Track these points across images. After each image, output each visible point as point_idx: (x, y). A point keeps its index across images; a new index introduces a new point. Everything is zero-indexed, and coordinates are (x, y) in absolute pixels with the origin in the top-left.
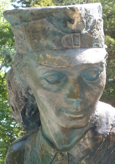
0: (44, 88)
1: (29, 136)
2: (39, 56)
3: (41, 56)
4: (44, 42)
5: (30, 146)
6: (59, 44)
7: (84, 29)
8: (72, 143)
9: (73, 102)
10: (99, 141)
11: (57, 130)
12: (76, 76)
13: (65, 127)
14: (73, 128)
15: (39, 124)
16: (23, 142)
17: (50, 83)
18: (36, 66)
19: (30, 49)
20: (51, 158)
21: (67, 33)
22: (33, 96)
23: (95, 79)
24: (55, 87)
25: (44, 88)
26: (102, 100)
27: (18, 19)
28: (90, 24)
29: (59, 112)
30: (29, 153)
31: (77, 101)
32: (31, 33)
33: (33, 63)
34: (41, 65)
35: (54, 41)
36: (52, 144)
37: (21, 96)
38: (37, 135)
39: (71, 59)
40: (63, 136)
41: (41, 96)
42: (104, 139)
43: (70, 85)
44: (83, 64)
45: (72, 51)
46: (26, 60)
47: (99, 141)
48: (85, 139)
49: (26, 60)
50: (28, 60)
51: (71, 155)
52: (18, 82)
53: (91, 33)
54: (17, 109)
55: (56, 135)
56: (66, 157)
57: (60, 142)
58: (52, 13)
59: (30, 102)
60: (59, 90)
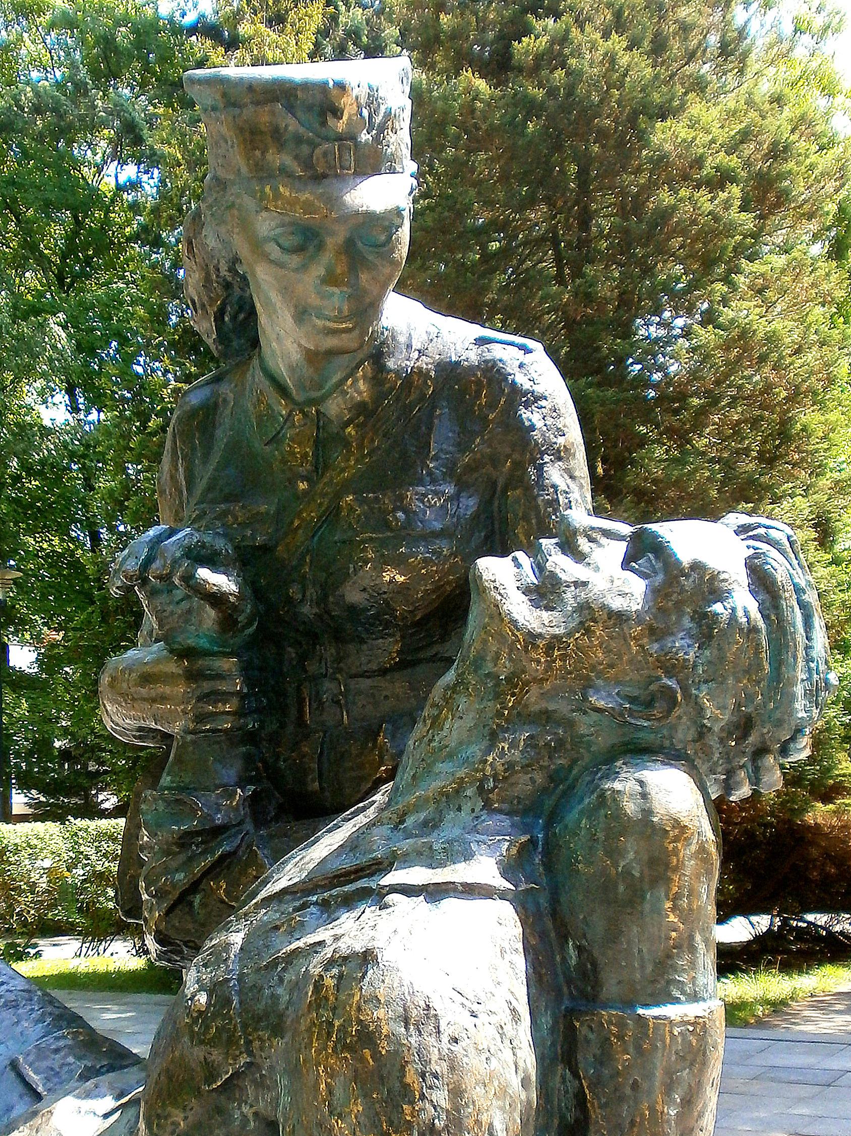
0: (271, 262)
1: (227, 372)
2: (264, 188)
3: (267, 189)
4: (276, 158)
5: (231, 395)
6: (308, 164)
7: (365, 131)
8: (327, 388)
9: (333, 294)
10: (387, 386)
11: (296, 356)
12: (340, 239)
13: (312, 348)
14: (331, 353)
15: (255, 343)
16: (211, 386)
17: (284, 249)
18: (257, 212)
19: (244, 170)
20: (278, 422)
21: (327, 139)
22: (244, 278)
23: (383, 245)
24: (295, 260)
25: (271, 262)
26: (401, 288)
27: (218, 97)
28: (378, 119)
29: (301, 314)
30: (228, 412)
31: (341, 292)
32: (247, 133)
33: (249, 203)
34: (266, 209)
35: (296, 157)
36: (282, 390)
37: (217, 276)
38: (248, 370)
39: (333, 202)
40: (308, 372)
41: (266, 277)
42: (399, 382)
43: (327, 257)
44: (357, 213)
45: (335, 181)
46: (232, 194)
47: (387, 386)
48: (355, 381)
49: (232, 194)
50: (238, 196)
51: (324, 415)
52: (212, 242)
53: (377, 140)
54: (203, 306)
55: (292, 369)
56: (313, 420)
57: (301, 386)
58: (295, 89)
59: (237, 291)
60: (303, 268)
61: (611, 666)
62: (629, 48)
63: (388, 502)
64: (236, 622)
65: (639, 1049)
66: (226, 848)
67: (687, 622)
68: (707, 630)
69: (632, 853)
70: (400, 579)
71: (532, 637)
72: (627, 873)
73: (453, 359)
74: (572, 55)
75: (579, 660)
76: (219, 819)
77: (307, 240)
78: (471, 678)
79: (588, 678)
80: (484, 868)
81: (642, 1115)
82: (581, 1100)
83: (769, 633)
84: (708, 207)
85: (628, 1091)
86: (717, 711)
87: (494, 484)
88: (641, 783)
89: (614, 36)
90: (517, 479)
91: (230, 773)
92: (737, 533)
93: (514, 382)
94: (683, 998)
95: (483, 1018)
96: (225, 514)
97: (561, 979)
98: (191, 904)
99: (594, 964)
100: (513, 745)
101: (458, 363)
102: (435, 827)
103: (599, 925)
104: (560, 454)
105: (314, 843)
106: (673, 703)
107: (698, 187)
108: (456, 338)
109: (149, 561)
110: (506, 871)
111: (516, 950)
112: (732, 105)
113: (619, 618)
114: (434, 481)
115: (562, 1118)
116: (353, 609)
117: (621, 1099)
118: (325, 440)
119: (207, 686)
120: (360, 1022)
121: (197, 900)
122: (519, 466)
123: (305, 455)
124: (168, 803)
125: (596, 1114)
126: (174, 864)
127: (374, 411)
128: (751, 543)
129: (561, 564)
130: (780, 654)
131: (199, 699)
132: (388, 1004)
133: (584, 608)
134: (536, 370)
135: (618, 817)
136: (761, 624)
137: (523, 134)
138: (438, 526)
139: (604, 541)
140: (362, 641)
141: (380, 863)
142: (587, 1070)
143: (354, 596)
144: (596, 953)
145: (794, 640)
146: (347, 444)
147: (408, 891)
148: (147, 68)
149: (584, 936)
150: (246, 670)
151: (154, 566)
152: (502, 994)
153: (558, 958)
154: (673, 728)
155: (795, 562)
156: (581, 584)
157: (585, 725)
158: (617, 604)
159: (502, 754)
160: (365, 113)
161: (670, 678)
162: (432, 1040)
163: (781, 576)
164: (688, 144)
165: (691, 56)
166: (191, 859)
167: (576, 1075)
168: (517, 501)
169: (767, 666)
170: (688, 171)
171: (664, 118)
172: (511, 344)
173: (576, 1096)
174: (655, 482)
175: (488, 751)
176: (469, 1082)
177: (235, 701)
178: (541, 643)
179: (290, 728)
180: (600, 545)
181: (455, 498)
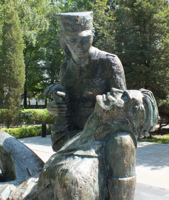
4: (69, 28)
6: (73, 29)
23: (88, 41)
24: (73, 44)
28: (85, 22)
35: (71, 28)
39: (77, 35)
40: (78, 60)
43: (77, 43)
48: (86, 61)
53: (85, 25)
55: (76, 59)
57: (77, 61)
62: (150, 4)
63: (90, 81)
65: (119, 185)
66: (63, 135)
67: (131, 109)
68: (135, 110)
69: (119, 151)
70: (91, 93)
71: (104, 110)
72: (118, 154)
74: (142, 5)
75: (112, 115)
76: (63, 130)
77: (74, 41)
79: (114, 118)
80: (93, 152)
81: (119, 197)
82: (109, 193)
83: (146, 111)
84: (162, 26)
86: (136, 124)
88: (121, 138)
89: (148, 2)
90: (111, 78)
91: (66, 123)
92: (142, 92)
93: (111, 62)
94: (127, 176)
95: (87, 183)
96: (66, 81)
97: (106, 171)
98: (58, 143)
100: (101, 129)
102: (87, 142)
104: (119, 74)
105: (72, 139)
106: (128, 123)
107: (160, 23)
109: (49, 91)
110: (96, 152)
112: (165, 12)
113: (119, 108)
114: (98, 78)
115: (106, 196)
116: (84, 97)
119: (61, 109)
120: (64, 183)
121: (59, 143)
122: (112, 75)
123: (78, 73)
125: (111, 196)
128: (144, 94)
129: (111, 97)
130: (148, 115)
131: (60, 111)
134: (117, 60)
136: (144, 110)
138: (98, 85)
139: (118, 93)
142: (110, 188)
143: (85, 96)
146: (85, 71)
147: (78, 156)
148: (86, 6)
149: (110, 164)
150: (68, 107)
151: (50, 91)
152: (92, 178)
153: (106, 168)
156: (113, 101)
157: (113, 126)
158: (119, 105)
161: (128, 119)
162: (76, 187)
163: (149, 101)
165: (160, 5)
166: (58, 136)
169: (145, 117)
170: (159, 21)
171: (155, 14)
172: (112, 56)
174: (154, 64)
175: (96, 129)
176: (83, 195)
177: (66, 111)
178: (106, 111)
180: (118, 94)
181: (101, 81)
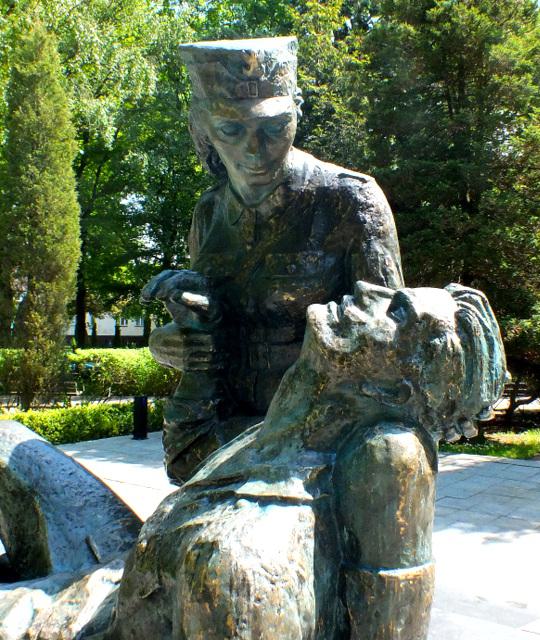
0: (221, 140)
6: (233, 92)
23: (280, 131)
24: (231, 139)
35: (228, 89)
36: (238, 197)
39: (246, 112)
43: (248, 138)
48: (275, 196)
55: (242, 189)
61: (376, 372)
62: (480, 13)
64: (208, 318)
65: (379, 592)
66: (202, 432)
67: (419, 349)
68: (430, 353)
69: (379, 482)
70: (292, 299)
71: (332, 353)
72: (376, 493)
73: (326, 185)
76: (200, 416)
77: (237, 130)
78: (303, 372)
79: (363, 378)
80: (296, 487)
83: (466, 356)
85: (373, 617)
86: (434, 398)
87: (344, 251)
88: (386, 442)
89: (473, 8)
90: (356, 248)
92: (453, 296)
93: (356, 199)
96: (212, 259)
97: (339, 548)
98: (185, 459)
99: (357, 542)
100: (321, 412)
101: (328, 188)
102: (277, 455)
103: (359, 523)
104: (381, 235)
105: (229, 446)
106: (409, 395)
107: (511, 75)
108: (330, 172)
109: (156, 290)
110: (308, 488)
111: (309, 537)
112: (529, 38)
113: (381, 345)
115: (338, 627)
116: (269, 312)
117: (369, 621)
118: (260, 225)
119: (195, 349)
120: (205, 586)
121: (188, 457)
122: (358, 242)
124: (176, 406)
126: (177, 438)
127: (284, 212)
128: (460, 302)
129: (353, 310)
132: (221, 576)
133: (362, 338)
134: (373, 194)
135: (372, 461)
136: (461, 351)
137: (430, 51)
138: (312, 272)
139: (378, 298)
140: (277, 328)
141: (242, 476)
143: (271, 306)
144: (358, 535)
145: (481, 359)
146: (270, 229)
147: (251, 498)
148: (274, 20)
150: (217, 342)
152: (293, 569)
153: (339, 537)
154: (411, 407)
155: (486, 313)
156: (362, 324)
157: (360, 402)
158: (379, 337)
159: (315, 417)
160: (264, 66)
161: (408, 380)
162: (244, 600)
163: (475, 323)
164: (507, 55)
165: (510, 17)
167: (345, 605)
168: (356, 259)
169: (464, 376)
170: (507, 68)
171: (496, 44)
172: (357, 178)
173: (344, 616)
176: (264, 625)
177: (210, 356)
178: (337, 357)
179: (243, 367)
181: (323, 258)
